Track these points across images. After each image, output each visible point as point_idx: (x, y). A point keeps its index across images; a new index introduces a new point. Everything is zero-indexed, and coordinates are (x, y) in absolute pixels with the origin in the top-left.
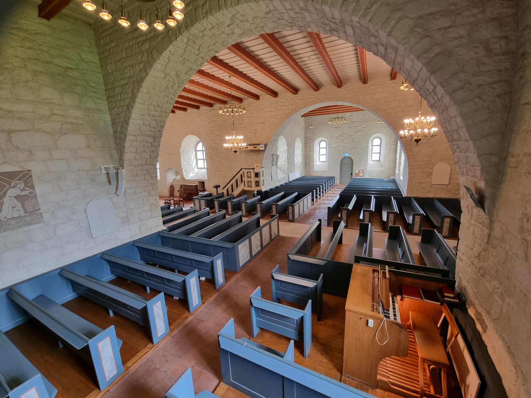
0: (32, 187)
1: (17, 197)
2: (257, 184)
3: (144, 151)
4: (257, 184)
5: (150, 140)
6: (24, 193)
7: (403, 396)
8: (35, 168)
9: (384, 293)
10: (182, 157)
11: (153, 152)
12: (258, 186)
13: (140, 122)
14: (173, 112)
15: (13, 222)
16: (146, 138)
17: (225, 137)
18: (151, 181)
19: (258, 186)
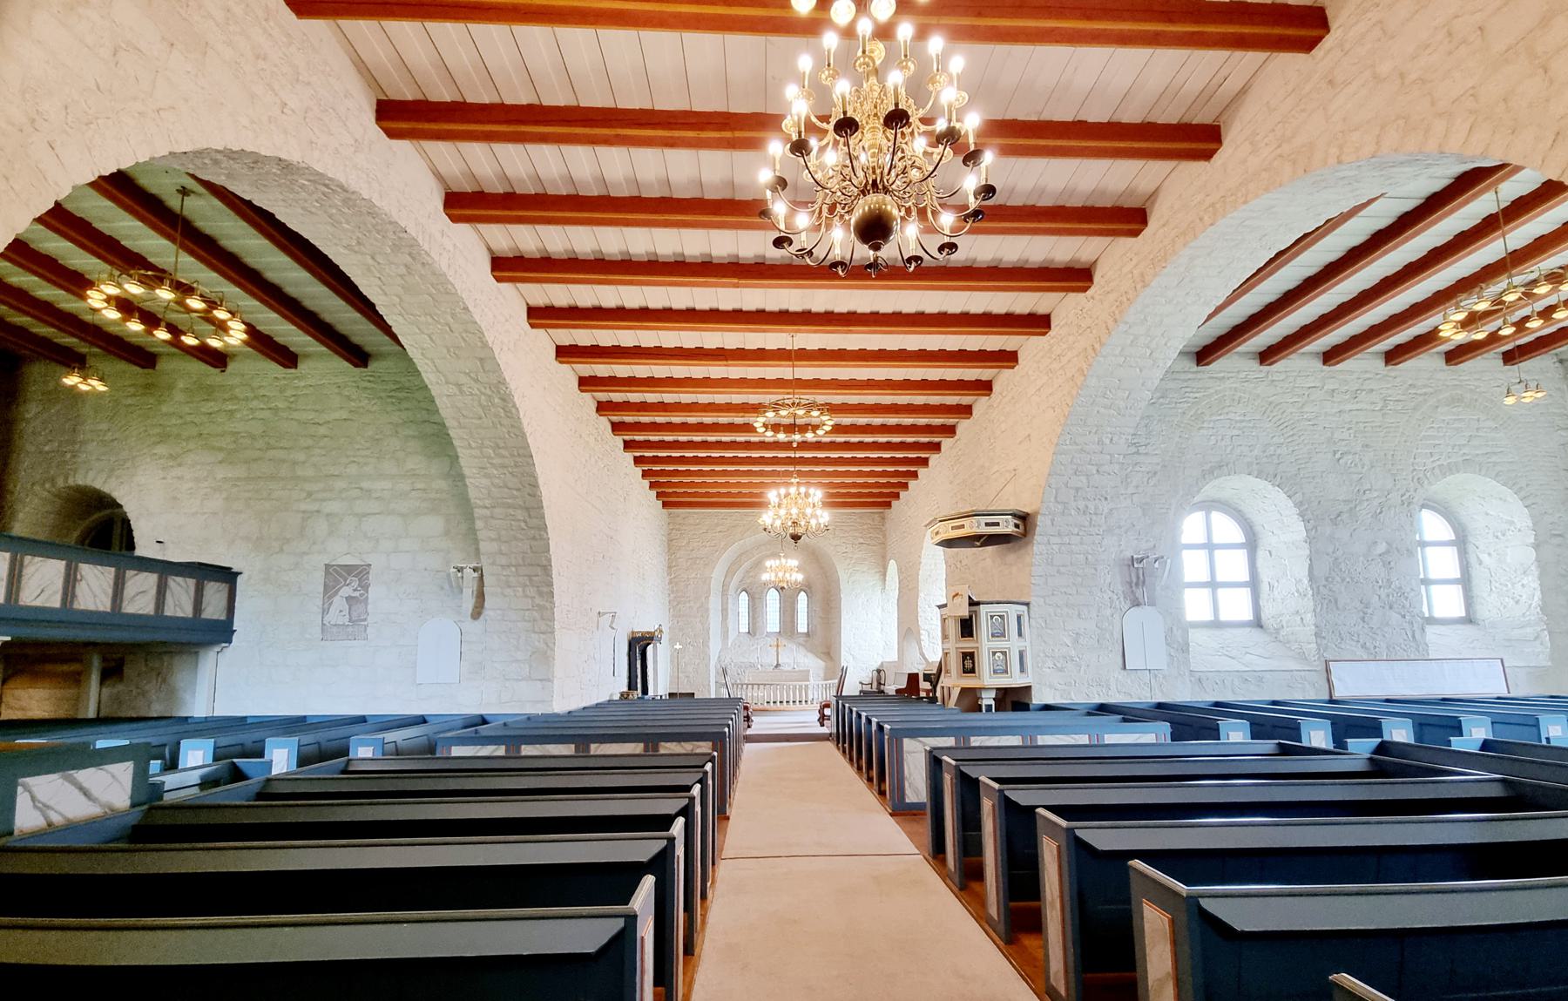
0: (366, 588)
1: (349, 599)
2: (968, 664)
3: (515, 538)
4: (968, 664)
5: (520, 514)
6: (357, 594)
7: (457, 6)
8: (376, 561)
9: (1084, 144)
10: (922, 595)
11: (534, 538)
12: (972, 671)
13: (485, 482)
14: (1024, 519)
15: (335, 630)
16: (511, 511)
17: (60, 378)
18: (538, 601)
19: (972, 671)
